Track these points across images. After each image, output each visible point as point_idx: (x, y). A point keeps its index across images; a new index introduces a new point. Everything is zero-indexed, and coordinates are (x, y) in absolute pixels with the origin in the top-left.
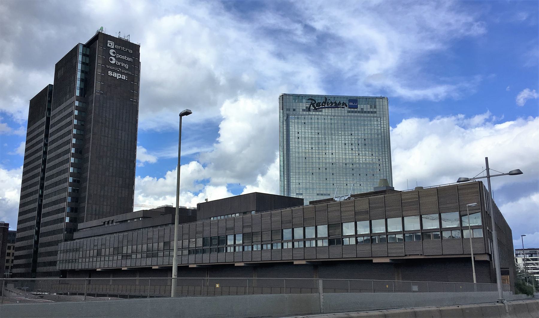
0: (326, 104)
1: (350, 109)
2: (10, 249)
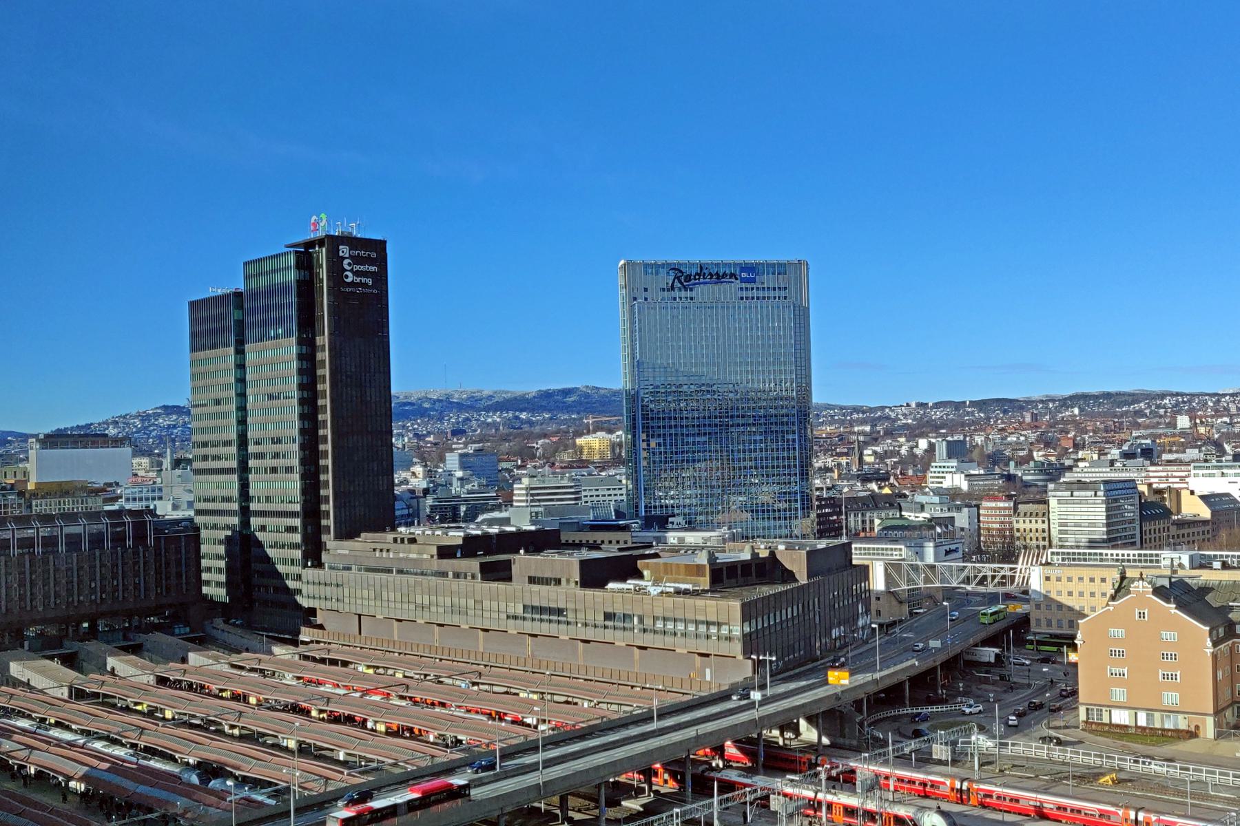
1: (744, 285)
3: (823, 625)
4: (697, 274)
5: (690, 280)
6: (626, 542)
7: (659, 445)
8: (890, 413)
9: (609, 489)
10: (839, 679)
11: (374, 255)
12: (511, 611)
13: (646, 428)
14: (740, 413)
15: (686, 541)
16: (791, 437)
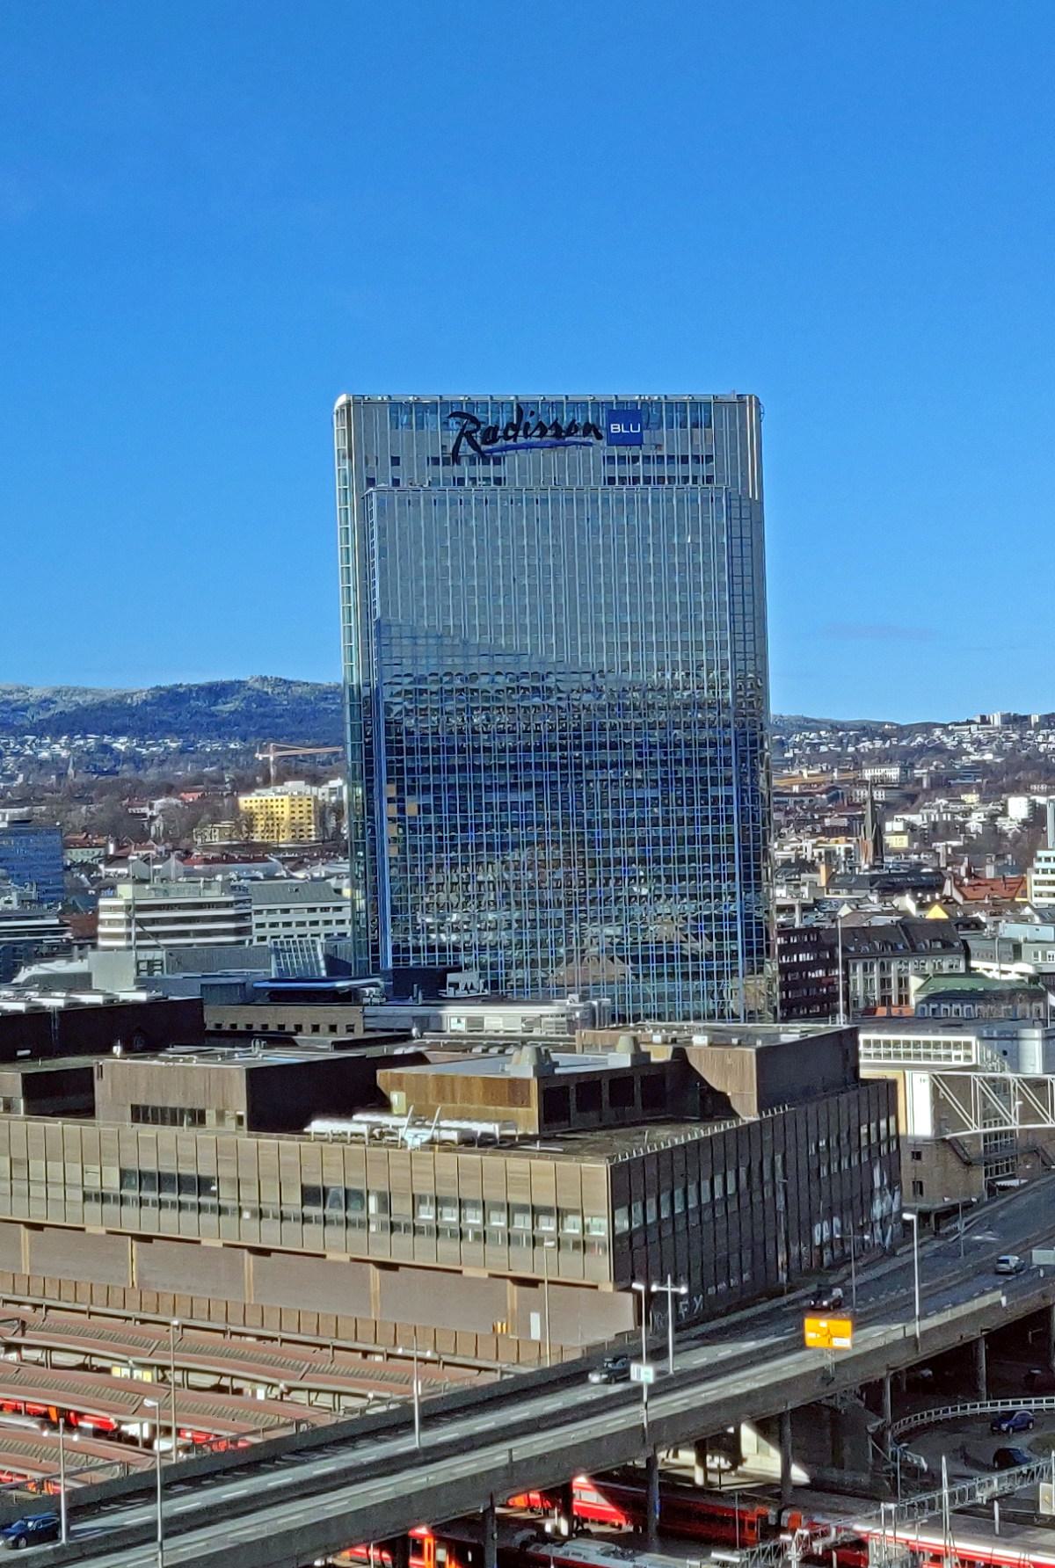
0: (521, 433)
2: (574, 1047)
3: (793, 1215)
4: (510, 425)
5: (495, 440)
7: (426, 809)
9: (313, 910)
12: (93, 1183)
13: (395, 772)
16: (721, 792)
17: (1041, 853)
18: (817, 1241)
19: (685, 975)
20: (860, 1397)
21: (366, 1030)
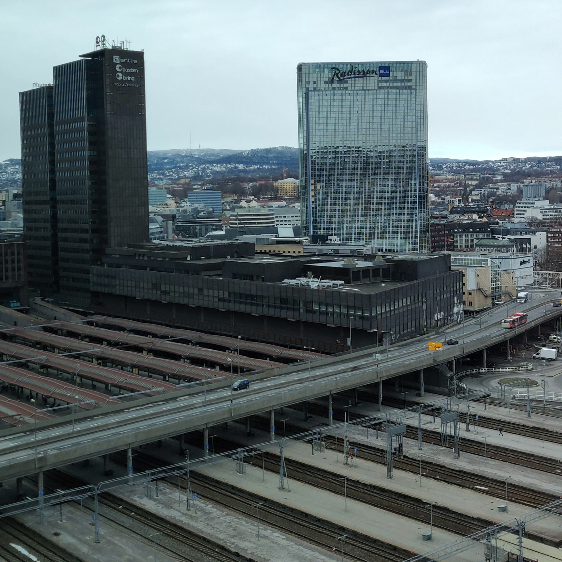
0: (353, 73)
1: (380, 78)
3: (429, 311)
4: (349, 71)
5: (345, 76)
6: (299, 252)
7: (322, 187)
8: (493, 165)
9: (293, 216)
10: (435, 347)
11: (136, 62)
12: (221, 296)
13: (314, 176)
14: (378, 166)
15: (340, 252)
16: (413, 182)
17: (518, 201)
18: (436, 319)
19: (401, 238)
20: (447, 366)
21: (304, 253)
